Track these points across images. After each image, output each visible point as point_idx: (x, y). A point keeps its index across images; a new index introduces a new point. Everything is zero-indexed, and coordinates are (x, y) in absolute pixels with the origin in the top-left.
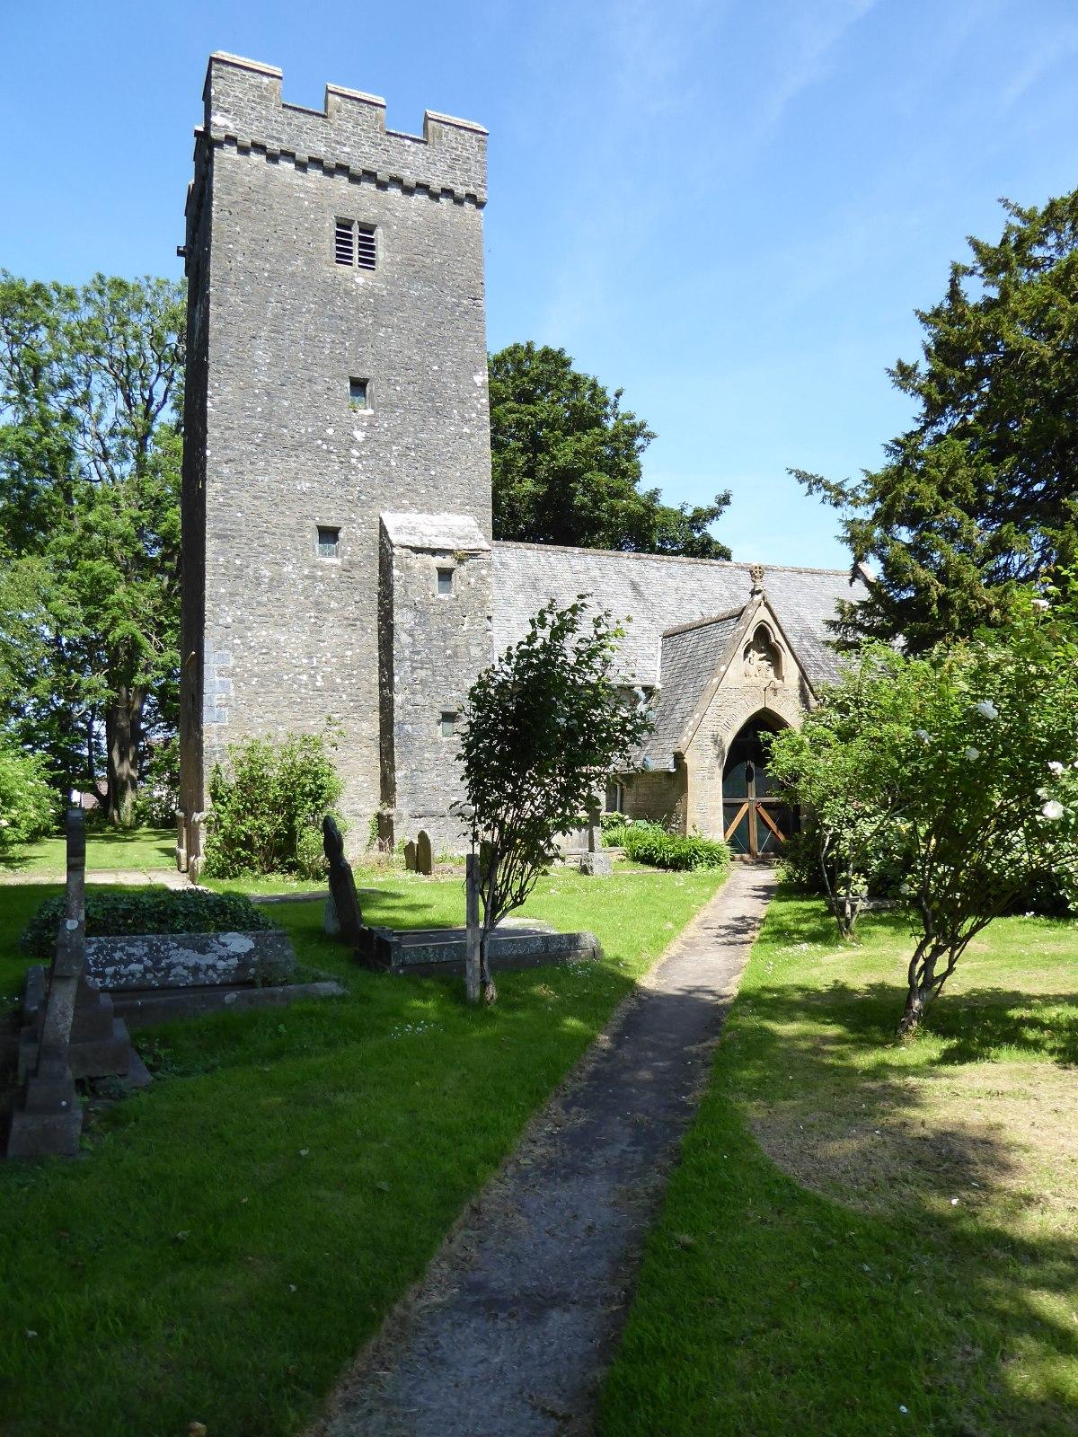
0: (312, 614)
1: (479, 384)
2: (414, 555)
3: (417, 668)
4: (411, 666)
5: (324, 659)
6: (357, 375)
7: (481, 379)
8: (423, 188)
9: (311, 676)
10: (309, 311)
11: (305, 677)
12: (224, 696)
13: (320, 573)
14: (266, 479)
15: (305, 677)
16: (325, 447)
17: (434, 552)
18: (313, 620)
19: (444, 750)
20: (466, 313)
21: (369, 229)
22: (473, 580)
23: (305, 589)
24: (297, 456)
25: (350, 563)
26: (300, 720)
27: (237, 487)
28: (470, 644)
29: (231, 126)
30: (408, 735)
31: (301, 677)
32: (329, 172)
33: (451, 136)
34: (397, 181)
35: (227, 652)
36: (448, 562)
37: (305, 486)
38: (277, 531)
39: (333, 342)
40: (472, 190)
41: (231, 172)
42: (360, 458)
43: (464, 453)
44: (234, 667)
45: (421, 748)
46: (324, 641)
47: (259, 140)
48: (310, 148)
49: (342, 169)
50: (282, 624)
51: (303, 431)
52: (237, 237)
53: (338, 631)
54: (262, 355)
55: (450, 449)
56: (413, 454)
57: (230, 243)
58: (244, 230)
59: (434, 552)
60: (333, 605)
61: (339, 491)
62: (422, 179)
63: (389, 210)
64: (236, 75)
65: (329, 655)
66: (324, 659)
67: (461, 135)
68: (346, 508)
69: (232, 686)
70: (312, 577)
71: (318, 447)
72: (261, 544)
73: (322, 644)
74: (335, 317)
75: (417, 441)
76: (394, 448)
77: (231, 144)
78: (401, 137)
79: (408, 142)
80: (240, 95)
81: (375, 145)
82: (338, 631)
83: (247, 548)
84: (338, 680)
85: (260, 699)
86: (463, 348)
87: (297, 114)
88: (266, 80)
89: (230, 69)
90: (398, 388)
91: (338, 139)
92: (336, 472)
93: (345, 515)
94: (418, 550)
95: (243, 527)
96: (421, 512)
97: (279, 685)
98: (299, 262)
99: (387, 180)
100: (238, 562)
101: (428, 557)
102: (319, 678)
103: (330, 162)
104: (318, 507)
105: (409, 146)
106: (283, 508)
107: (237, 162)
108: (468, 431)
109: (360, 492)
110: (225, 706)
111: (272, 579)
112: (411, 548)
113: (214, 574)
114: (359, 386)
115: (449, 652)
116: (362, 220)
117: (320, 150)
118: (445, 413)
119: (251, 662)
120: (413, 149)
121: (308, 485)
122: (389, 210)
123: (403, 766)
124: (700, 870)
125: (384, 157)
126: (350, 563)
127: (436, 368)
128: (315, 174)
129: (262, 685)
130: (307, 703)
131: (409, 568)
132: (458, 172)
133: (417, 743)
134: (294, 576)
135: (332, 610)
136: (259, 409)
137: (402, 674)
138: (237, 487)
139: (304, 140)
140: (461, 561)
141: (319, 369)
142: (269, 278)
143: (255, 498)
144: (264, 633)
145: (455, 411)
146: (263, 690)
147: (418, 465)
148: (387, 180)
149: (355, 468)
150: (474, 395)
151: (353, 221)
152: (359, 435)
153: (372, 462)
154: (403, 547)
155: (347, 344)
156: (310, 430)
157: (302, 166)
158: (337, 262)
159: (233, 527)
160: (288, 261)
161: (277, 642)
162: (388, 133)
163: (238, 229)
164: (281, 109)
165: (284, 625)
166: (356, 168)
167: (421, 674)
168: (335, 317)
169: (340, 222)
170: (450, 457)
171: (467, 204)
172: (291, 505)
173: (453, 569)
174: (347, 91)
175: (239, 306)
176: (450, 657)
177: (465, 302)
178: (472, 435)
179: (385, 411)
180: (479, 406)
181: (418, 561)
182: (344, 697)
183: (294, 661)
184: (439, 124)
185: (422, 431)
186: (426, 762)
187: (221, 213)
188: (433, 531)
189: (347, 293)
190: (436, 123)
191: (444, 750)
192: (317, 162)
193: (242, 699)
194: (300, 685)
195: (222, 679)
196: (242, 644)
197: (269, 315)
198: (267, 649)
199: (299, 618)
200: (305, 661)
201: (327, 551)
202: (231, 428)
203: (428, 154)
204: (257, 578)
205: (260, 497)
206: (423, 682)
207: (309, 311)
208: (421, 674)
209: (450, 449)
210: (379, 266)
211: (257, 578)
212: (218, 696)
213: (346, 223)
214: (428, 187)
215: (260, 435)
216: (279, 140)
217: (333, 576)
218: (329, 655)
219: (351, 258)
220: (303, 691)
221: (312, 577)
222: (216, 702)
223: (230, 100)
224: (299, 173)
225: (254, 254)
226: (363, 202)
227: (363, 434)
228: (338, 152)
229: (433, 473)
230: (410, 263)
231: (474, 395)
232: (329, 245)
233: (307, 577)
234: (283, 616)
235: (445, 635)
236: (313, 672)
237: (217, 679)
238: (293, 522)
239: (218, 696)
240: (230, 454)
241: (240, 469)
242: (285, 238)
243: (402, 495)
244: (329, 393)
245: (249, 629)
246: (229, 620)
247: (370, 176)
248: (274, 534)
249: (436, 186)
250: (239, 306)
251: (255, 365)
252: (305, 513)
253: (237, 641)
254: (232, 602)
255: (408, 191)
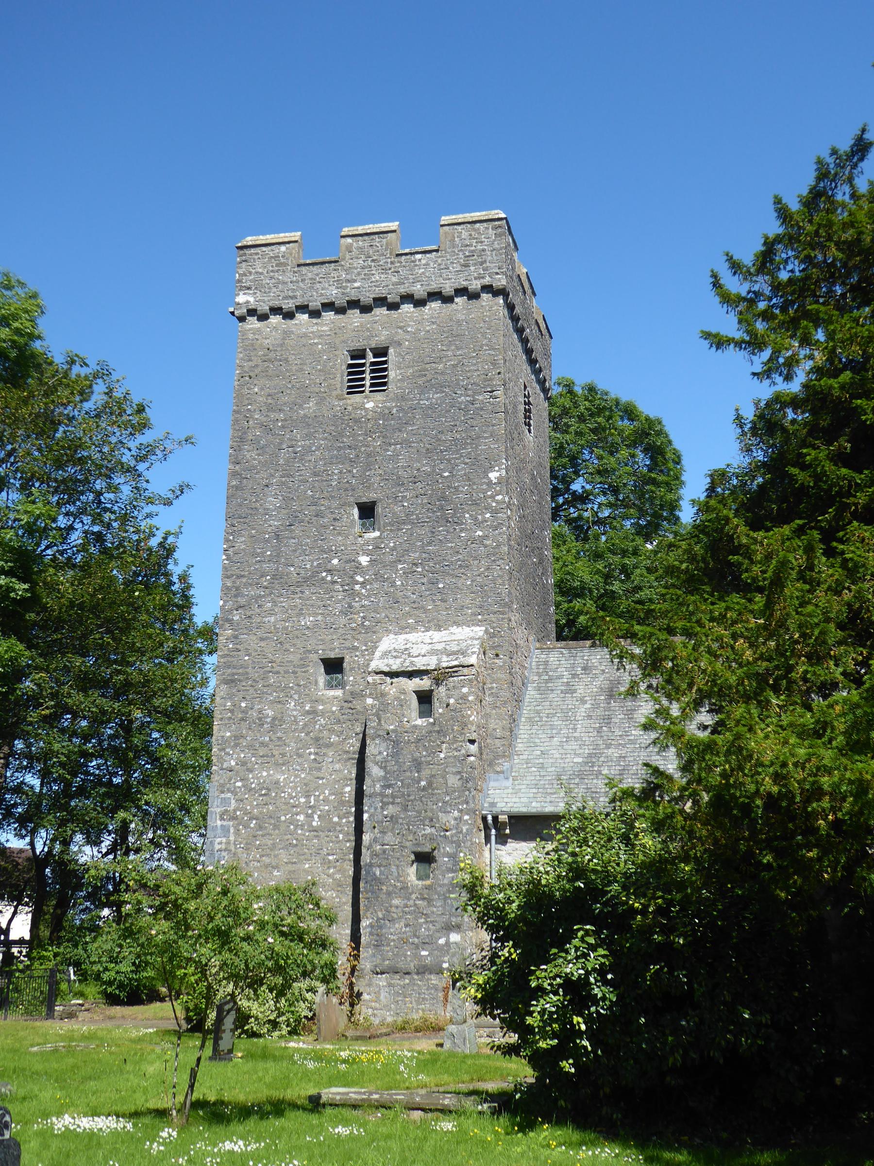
0: (312, 750)
1: (495, 481)
2: (388, 679)
3: (388, 804)
4: (382, 801)
5: (321, 797)
6: (364, 500)
7: (497, 474)
8: (435, 295)
9: (308, 816)
10: (318, 449)
11: (301, 817)
12: (224, 840)
13: (321, 707)
14: (272, 619)
15: (301, 817)
16: (329, 578)
17: (410, 675)
18: (312, 757)
19: (414, 896)
20: (482, 409)
21: (382, 351)
22: (452, 701)
23: (305, 725)
24: (302, 592)
25: (352, 693)
26: (295, 863)
27: (245, 631)
28: (447, 773)
29: (251, 299)
30: (375, 878)
31: (298, 817)
32: (341, 311)
33: (465, 235)
34: (408, 298)
35: (229, 795)
36: (425, 683)
37: (309, 621)
38: (281, 669)
39: (341, 472)
40: (487, 281)
41: (253, 340)
42: (363, 584)
43: (475, 558)
44: (235, 811)
45: (389, 894)
46: (323, 778)
47: (276, 303)
48: (322, 295)
49: (354, 304)
50: (282, 763)
51: (308, 566)
52: (255, 397)
53: (337, 766)
54: (272, 501)
55: (460, 557)
56: (419, 570)
57: (249, 404)
58: (262, 389)
59: (410, 675)
60: (334, 738)
61: (343, 620)
62: (434, 287)
63: (401, 328)
64: (257, 254)
65: (327, 792)
66: (321, 797)
67: (475, 230)
68: (349, 637)
69: (232, 830)
70: (313, 712)
71: (323, 579)
72: (266, 684)
73: (321, 782)
74: (344, 448)
75: (424, 555)
76: (400, 566)
77: (253, 316)
78: (411, 254)
79: (418, 256)
80: (260, 270)
81: (385, 270)
82: (337, 766)
83: (252, 691)
84: (336, 819)
85: (258, 842)
86: (477, 447)
87: (323, 269)
88: (283, 248)
89: (253, 251)
90: (406, 504)
91: (349, 277)
92: (340, 601)
93: (348, 644)
94: (393, 675)
95: (250, 670)
96: (428, 630)
97: (276, 827)
98: (311, 404)
99: (398, 299)
100: (243, 705)
101: (403, 680)
102: (316, 817)
103: (341, 302)
104: (322, 640)
105: (420, 260)
106: (287, 646)
107: (259, 330)
108: (480, 533)
109: (364, 618)
110: (225, 850)
111: (274, 719)
112: (386, 674)
113: (221, 719)
114: (367, 511)
115: (423, 783)
116: (373, 346)
117: (333, 293)
118: (456, 520)
119: (252, 805)
120: (423, 262)
121: (311, 619)
122: (401, 328)
123: (368, 915)
124: (127, 1112)
125: (394, 279)
126: (352, 693)
127: (446, 474)
128: (329, 316)
129: (260, 828)
130: (302, 845)
131: (383, 695)
132: (472, 268)
133: (384, 888)
134: (295, 713)
135: (332, 744)
136: (269, 553)
137: (372, 810)
138: (245, 631)
139: (317, 291)
140: (438, 682)
141: (326, 503)
142: (283, 427)
143: (262, 639)
144: (265, 774)
145: (467, 516)
146: (261, 833)
147: (425, 580)
148: (398, 299)
149: (359, 594)
150: (489, 493)
151: (365, 350)
152: (364, 560)
153: (376, 585)
154: (377, 673)
155: (355, 471)
156: (315, 564)
157: (315, 314)
158: (349, 393)
159: (241, 671)
160: (301, 406)
161: (277, 782)
162: (398, 255)
163: (256, 390)
164: (296, 269)
165: (283, 764)
166: (367, 298)
167: (390, 810)
168: (344, 448)
169: (353, 353)
170: (460, 566)
171: (484, 296)
172: (294, 642)
173: (432, 691)
174: (360, 229)
175: (255, 459)
176: (424, 789)
177: (481, 398)
178: (486, 537)
179: (391, 530)
180: (494, 504)
181: (392, 688)
182: (341, 836)
183: (292, 801)
184: (451, 227)
185: (429, 544)
186: (394, 909)
187: (242, 380)
188: (424, 649)
189: (357, 421)
190: (448, 227)
191: (414, 896)
192: (329, 306)
193: (241, 843)
194: (296, 826)
195: (225, 823)
196: (243, 786)
197: (281, 462)
198: (269, 789)
199: (300, 756)
200: (302, 800)
201: (334, 683)
202: (243, 576)
203: (439, 261)
204: (260, 719)
205: (267, 638)
206: (393, 819)
207: (318, 449)
208: (390, 810)
209: (460, 557)
210: (391, 386)
211: (260, 719)
212: (219, 840)
213: (360, 353)
214: (412, 296)
215: (268, 577)
216: (295, 297)
217: (334, 709)
218: (327, 792)
219: (363, 386)
220: (300, 832)
221: (313, 712)
222: (217, 847)
223: (252, 277)
224: (315, 321)
225: (270, 409)
226: (377, 327)
227: (368, 559)
228: (348, 290)
229: (441, 586)
230: (422, 373)
231: (489, 493)
232: (341, 378)
233: (308, 713)
234: (283, 755)
235: (418, 765)
236: (310, 812)
237: (219, 823)
238: (295, 658)
239: (219, 840)
240: (242, 601)
241: (249, 613)
242: (298, 385)
243: (409, 615)
244: (337, 524)
245: (251, 771)
246: (233, 763)
247: (381, 301)
248: (278, 672)
249: (448, 289)
250: (255, 459)
251: (267, 511)
252: (309, 648)
253: (239, 784)
254: (236, 745)
255: (420, 303)
